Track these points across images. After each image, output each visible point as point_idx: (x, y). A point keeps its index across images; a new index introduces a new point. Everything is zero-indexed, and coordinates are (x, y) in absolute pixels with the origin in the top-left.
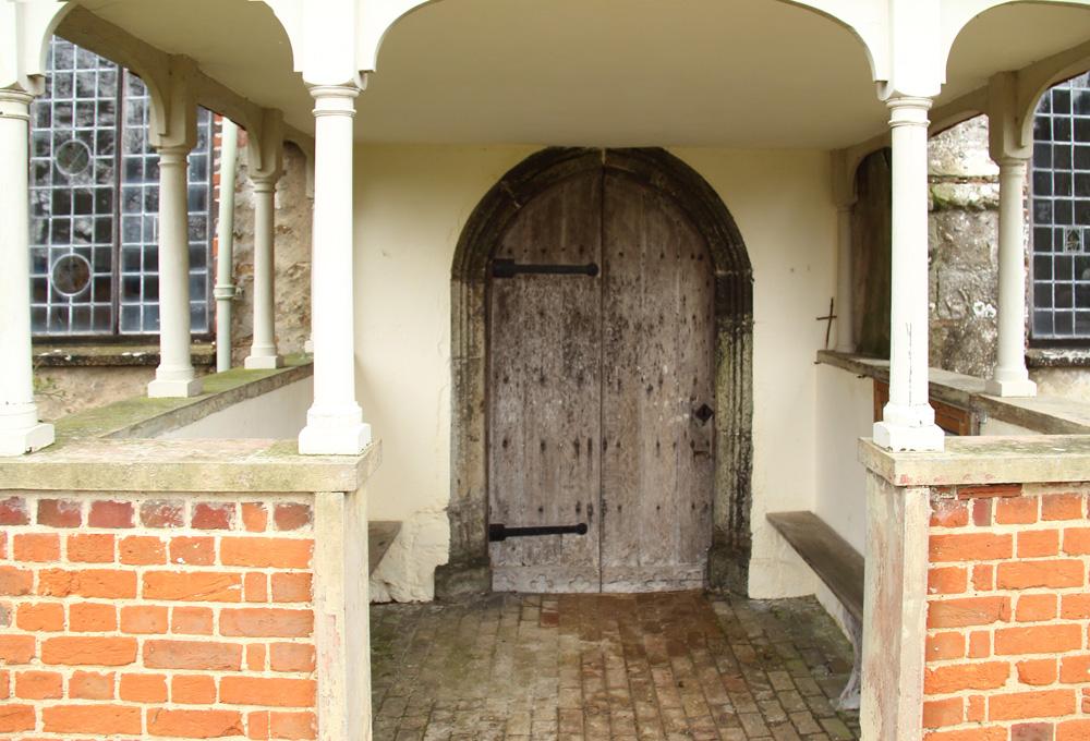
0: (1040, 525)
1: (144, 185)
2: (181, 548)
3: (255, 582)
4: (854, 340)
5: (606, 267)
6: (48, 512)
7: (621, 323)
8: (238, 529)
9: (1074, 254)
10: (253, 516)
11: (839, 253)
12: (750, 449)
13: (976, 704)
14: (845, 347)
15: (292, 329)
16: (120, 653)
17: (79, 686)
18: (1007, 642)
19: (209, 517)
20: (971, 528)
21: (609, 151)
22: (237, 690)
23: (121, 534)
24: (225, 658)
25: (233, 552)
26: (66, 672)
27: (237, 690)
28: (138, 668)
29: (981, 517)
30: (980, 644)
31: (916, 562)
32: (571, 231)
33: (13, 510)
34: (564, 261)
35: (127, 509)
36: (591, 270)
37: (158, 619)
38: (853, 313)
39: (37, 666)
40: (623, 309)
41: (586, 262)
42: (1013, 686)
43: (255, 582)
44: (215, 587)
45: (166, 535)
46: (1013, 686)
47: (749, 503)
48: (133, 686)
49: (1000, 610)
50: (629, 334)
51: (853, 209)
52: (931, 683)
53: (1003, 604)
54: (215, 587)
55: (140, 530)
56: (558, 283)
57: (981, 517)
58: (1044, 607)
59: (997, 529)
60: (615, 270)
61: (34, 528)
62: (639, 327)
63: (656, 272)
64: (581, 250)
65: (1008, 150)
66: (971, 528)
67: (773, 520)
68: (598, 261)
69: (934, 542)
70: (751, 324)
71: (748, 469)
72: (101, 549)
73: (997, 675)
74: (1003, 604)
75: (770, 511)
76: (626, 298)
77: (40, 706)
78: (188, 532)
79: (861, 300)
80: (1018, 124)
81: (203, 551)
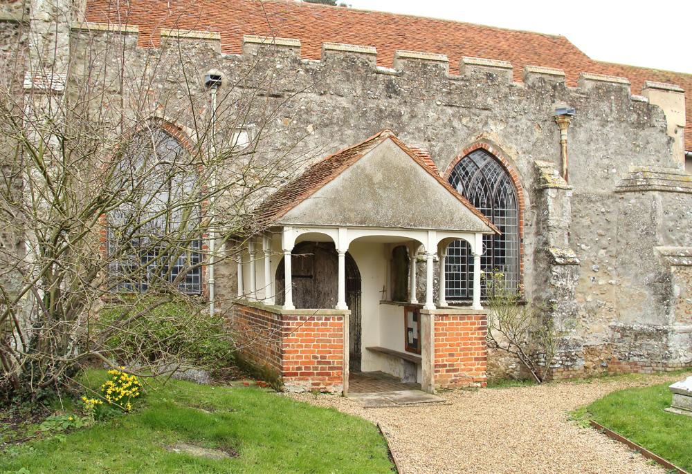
0: (452, 321)
1: (448, 289)
2: (323, 324)
3: (334, 329)
4: (391, 297)
5: (315, 276)
6: (301, 319)
7: (319, 293)
8: (331, 321)
9: (455, 272)
10: (334, 319)
11: (387, 270)
12: (360, 329)
13: (442, 349)
14: (389, 299)
15: (230, 293)
16: (313, 341)
17: (306, 346)
18: (447, 340)
19: (327, 319)
20: (441, 321)
21: (319, 243)
22: (331, 347)
23: (313, 322)
24: (329, 341)
25: (331, 324)
26: (304, 344)
27: (331, 347)
28: (315, 343)
29: (442, 320)
30: (443, 340)
31: (433, 326)
32: (305, 265)
33: (18, 370)
34: (303, 274)
35: (314, 318)
36: (311, 277)
37: (318, 335)
38: (391, 290)
39: (299, 343)
40: (320, 289)
41: (309, 274)
42: (448, 347)
43: (334, 329)
44: (328, 330)
45: (320, 322)
46: (448, 347)
47: (360, 344)
48: (315, 346)
49: (446, 335)
50: (322, 296)
51: (391, 261)
52: (436, 346)
53: (446, 334)
54: (328, 330)
55: (316, 321)
56: (301, 281)
57: (442, 320)
58: (453, 334)
59: (444, 322)
60: (318, 277)
61: (299, 321)
62: (325, 294)
63: (330, 278)
64: (308, 271)
65: (442, 254)
66: (441, 321)
67: (367, 349)
68: (313, 274)
69: (435, 323)
70: (361, 293)
71: (360, 334)
72: (310, 324)
73: (445, 345)
74: (446, 334)
75: (368, 346)
76: (321, 285)
77: (299, 350)
78: (323, 321)
79: (393, 287)
80: (444, 249)
81: (326, 324)
